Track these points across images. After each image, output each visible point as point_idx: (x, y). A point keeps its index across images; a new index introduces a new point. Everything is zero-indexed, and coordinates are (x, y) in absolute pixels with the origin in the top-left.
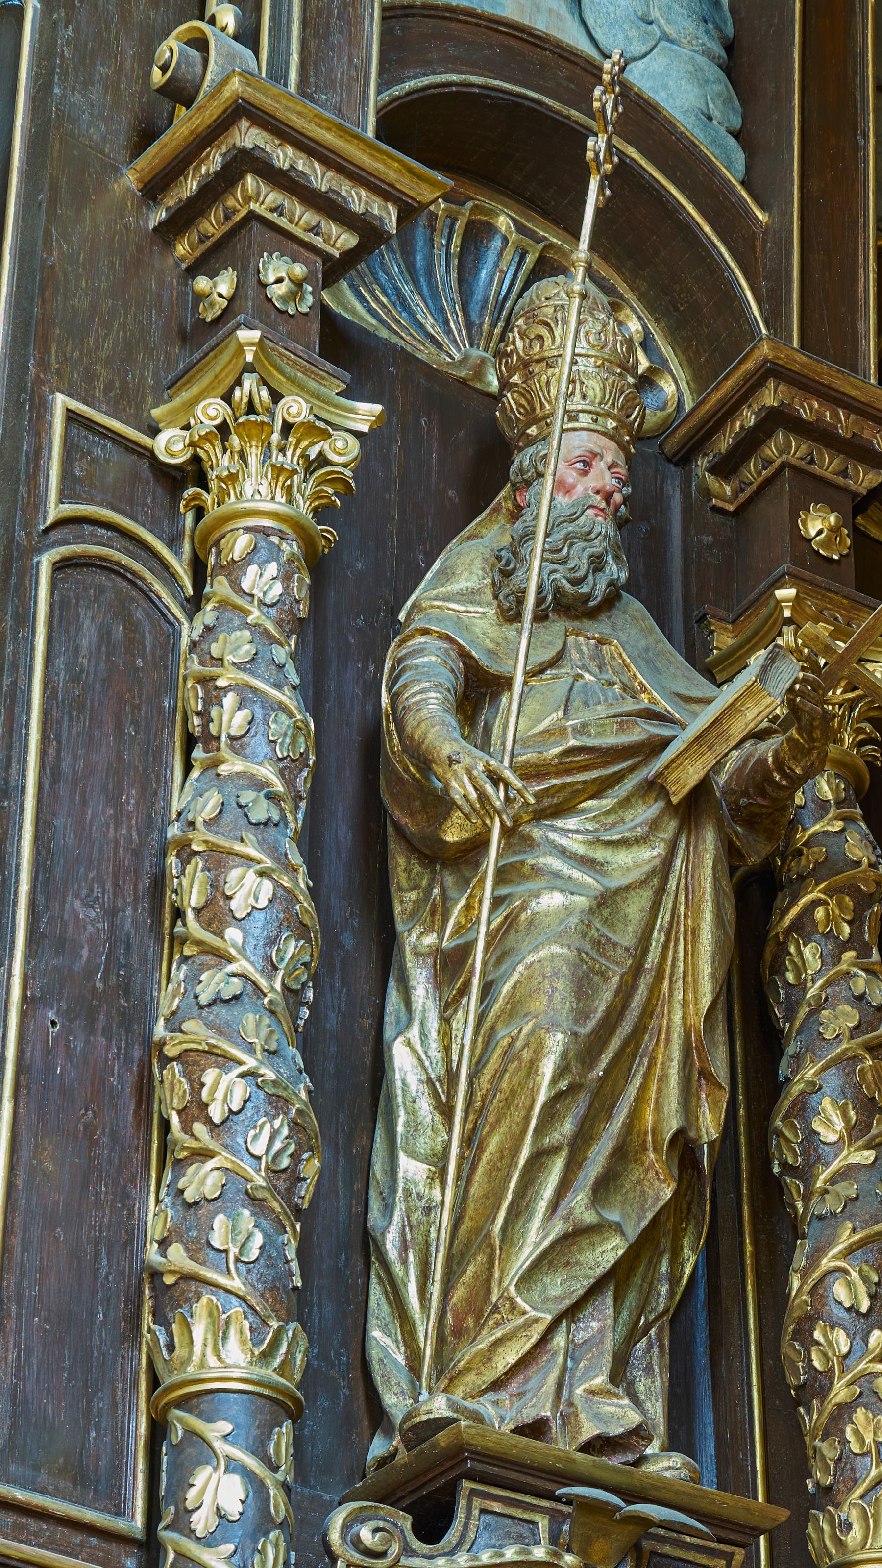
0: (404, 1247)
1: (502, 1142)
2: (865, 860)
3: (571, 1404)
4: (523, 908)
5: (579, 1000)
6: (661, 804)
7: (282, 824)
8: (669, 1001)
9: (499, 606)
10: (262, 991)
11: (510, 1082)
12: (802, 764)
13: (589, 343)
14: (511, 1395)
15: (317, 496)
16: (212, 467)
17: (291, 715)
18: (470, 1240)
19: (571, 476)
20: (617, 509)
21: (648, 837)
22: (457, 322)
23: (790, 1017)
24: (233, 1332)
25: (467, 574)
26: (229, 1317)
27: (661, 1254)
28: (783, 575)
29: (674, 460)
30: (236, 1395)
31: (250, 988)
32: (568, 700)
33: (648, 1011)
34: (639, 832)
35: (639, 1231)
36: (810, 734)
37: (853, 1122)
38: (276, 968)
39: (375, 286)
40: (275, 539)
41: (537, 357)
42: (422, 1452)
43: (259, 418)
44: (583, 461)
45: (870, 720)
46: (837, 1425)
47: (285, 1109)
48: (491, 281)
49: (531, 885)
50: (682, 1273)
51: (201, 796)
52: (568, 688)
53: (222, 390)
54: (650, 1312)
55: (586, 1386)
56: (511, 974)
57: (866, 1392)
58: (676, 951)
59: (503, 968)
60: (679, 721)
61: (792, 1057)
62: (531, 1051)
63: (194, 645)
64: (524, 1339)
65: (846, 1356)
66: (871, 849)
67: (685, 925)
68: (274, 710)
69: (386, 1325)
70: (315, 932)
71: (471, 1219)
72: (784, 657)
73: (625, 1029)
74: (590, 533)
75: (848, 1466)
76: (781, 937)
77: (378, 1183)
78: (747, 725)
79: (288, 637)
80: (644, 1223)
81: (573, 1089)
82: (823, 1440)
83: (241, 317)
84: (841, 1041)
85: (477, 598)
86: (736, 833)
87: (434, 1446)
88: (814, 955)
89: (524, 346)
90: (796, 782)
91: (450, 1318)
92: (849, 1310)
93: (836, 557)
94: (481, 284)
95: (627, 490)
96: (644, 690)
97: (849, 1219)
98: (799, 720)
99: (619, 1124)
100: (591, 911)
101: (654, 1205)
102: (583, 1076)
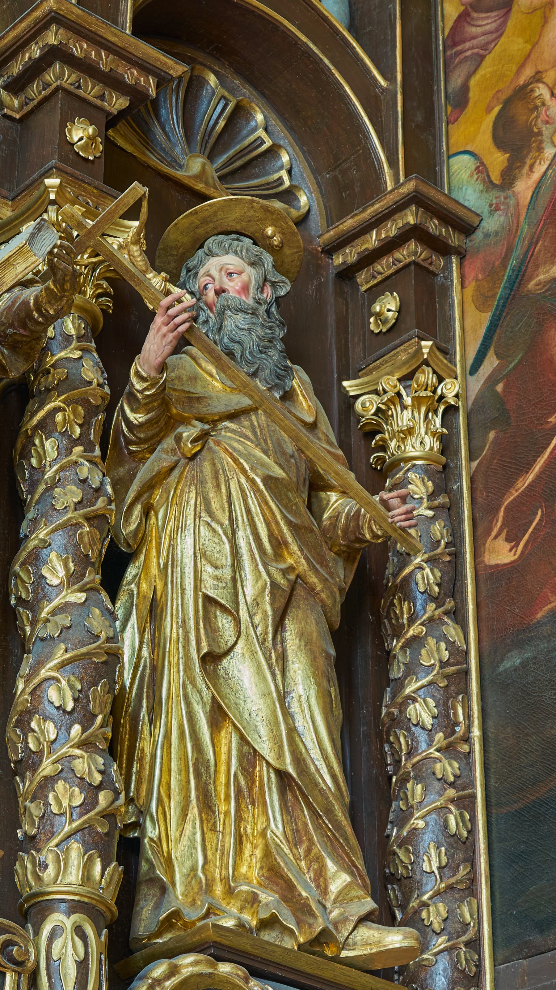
28: (51, 168)
36: (62, 286)
37: (72, 571)
45: (107, 279)
46: (43, 792)
57: (66, 769)
61: (31, 520)
65: (53, 742)
66: (100, 373)
75: (49, 822)
76: (29, 432)
78: (17, 275)
82: (31, 802)
84: (67, 511)
88: (53, 447)
90: (50, 320)
92: (58, 708)
93: (91, 158)
98: (55, 274)
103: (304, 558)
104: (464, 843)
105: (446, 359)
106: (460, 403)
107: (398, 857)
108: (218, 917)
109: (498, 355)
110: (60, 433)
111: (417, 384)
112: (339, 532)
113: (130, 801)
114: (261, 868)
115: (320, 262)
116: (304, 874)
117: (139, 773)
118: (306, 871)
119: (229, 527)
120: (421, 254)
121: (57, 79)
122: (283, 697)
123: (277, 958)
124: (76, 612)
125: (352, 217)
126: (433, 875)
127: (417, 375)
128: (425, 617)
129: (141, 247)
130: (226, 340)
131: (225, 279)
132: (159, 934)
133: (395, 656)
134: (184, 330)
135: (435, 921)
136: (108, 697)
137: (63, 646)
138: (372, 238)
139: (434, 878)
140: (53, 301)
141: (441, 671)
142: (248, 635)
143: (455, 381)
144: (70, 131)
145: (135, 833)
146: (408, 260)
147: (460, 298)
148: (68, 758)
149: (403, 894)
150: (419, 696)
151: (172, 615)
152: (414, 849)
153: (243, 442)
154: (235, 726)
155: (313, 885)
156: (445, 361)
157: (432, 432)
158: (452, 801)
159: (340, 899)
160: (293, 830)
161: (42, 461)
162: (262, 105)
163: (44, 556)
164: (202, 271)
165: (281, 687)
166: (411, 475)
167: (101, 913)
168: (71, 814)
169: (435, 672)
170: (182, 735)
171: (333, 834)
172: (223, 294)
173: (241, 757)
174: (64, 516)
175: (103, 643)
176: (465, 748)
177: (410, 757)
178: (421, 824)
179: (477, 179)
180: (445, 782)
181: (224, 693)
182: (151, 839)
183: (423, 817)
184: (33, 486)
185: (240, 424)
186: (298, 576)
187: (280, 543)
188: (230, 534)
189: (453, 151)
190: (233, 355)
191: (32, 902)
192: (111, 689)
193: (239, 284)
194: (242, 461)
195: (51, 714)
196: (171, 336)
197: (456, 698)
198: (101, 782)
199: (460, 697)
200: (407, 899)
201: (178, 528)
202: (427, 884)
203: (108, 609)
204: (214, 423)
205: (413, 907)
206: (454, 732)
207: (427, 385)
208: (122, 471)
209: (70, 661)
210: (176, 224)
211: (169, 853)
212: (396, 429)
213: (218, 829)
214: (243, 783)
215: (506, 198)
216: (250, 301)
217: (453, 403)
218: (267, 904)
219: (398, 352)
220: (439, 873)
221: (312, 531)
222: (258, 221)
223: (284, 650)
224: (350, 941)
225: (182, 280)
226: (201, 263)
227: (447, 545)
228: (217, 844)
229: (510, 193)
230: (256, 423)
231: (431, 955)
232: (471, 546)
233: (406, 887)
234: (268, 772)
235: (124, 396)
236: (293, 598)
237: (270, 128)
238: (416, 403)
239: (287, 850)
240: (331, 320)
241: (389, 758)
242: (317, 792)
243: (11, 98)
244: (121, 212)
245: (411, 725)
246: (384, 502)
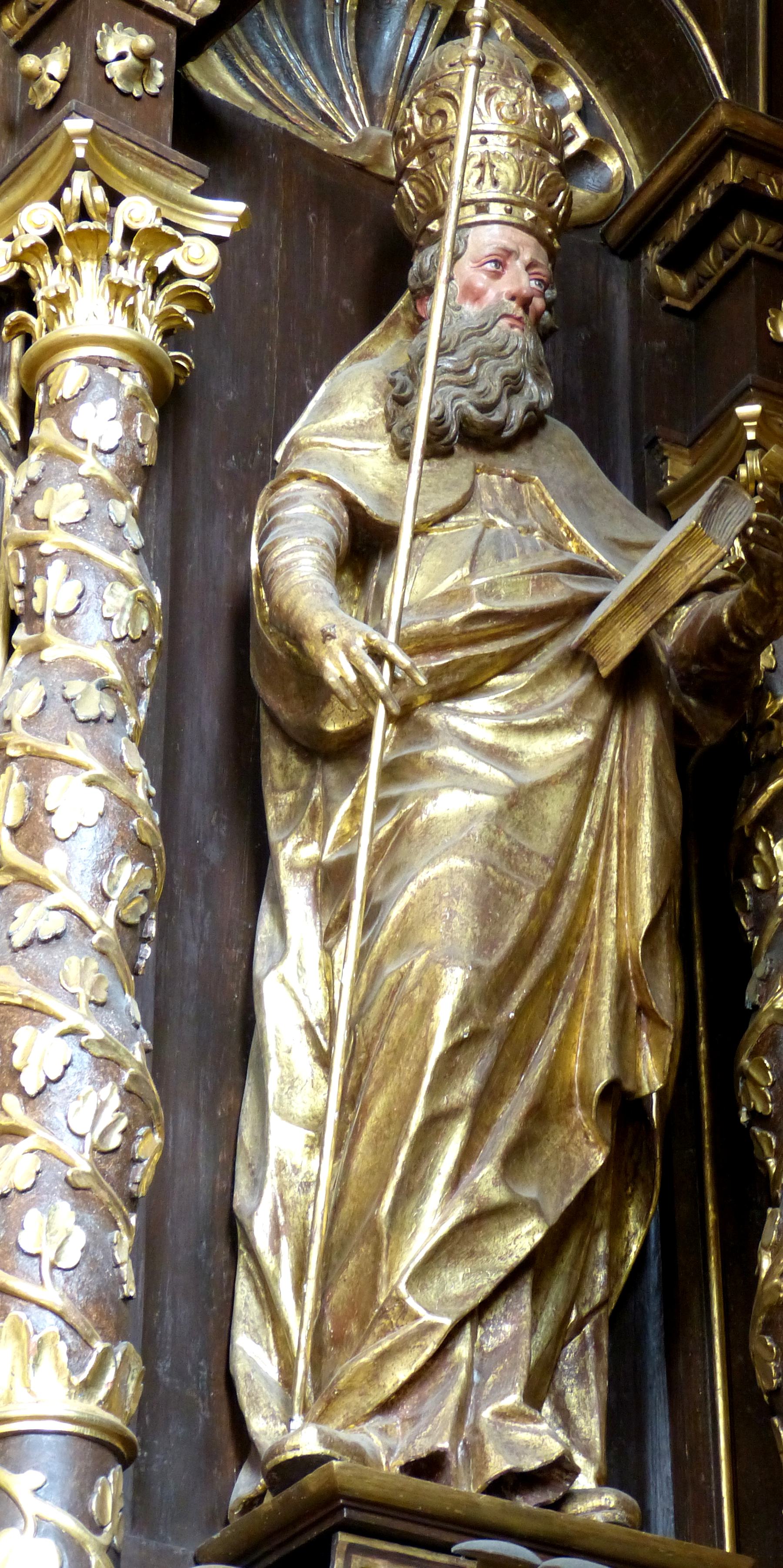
0: (276, 1233)
1: (389, 1103)
3: (476, 1430)
4: (417, 812)
5: (483, 925)
6: (588, 678)
7: (118, 720)
8: (600, 920)
9: (393, 441)
10: (90, 928)
11: (399, 1029)
13: (501, 117)
14: (404, 1420)
15: (167, 316)
16: (40, 286)
17: (130, 585)
18: (352, 1226)
19: (481, 280)
20: (538, 317)
21: (571, 718)
22: (354, 96)
23: (759, 929)
24: (47, 1355)
25: (355, 402)
26: (41, 1339)
27: (597, 1232)
28: (747, 388)
29: (619, 251)
30: (49, 1438)
31: (75, 924)
32: (475, 553)
33: (572, 934)
34: (561, 714)
35: (562, 1209)
36: (771, 586)
38: (107, 899)
39: (254, 57)
40: (114, 371)
41: (438, 137)
42: (287, 1499)
43: (92, 225)
44: (495, 261)
47: (115, 1073)
48: (396, 44)
49: (427, 784)
50: (628, 1250)
51: (20, 688)
52: (475, 538)
53: (51, 192)
54: (584, 1305)
55: (494, 1407)
56: (401, 895)
58: (608, 858)
59: (394, 885)
60: (613, 573)
62: (424, 991)
63: (17, 502)
64: (417, 1350)
67: (619, 826)
68: (109, 580)
69: (255, 1331)
70: (159, 852)
71: (354, 1200)
72: (736, 493)
73: (543, 958)
74: (503, 348)
76: (747, 831)
77: (247, 1153)
78: (688, 579)
79: (130, 489)
80: (570, 1198)
81: (476, 1036)
83: (72, 104)
85: (367, 431)
86: (688, 706)
87: (303, 1490)
89: (424, 124)
91: (329, 1326)
94: (384, 48)
95: (551, 294)
96: (571, 536)
98: (757, 569)
99: (537, 1076)
100: (500, 813)
101: (581, 1174)
102: (489, 1019)
121: (745, 239)
161: (771, 878)
184: (760, 921)
243: (675, 279)
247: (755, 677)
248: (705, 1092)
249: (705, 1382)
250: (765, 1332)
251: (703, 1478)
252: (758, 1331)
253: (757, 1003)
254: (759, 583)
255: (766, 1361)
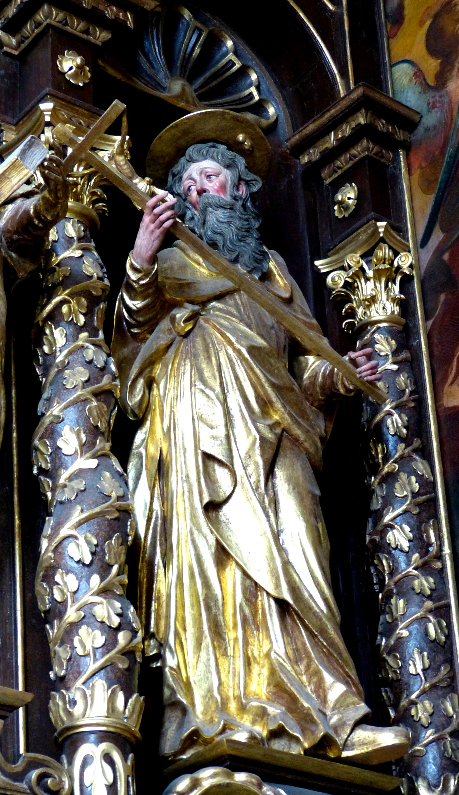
2: (95, 275)
12: (52, 213)
23: (45, 375)
36: (56, 194)
37: (84, 441)
45: (101, 187)
46: (69, 636)
57: (88, 615)
61: (46, 400)
65: (75, 592)
66: (99, 268)
75: (76, 663)
76: (40, 324)
78: (12, 187)
82: (60, 646)
84: (77, 390)
86: (11, 257)
88: (61, 335)
90: (48, 225)
92: (78, 562)
93: (81, 84)
97: (79, 503)
103: (288, 414)
104: (443, 647)
105: (400, 236)
106: (414, 272)
107: (388, 663)
108: (234, 731)
109: (443, 229)
110: (67, 322)
111: (376, 259)
112: (318, 389)
113: (149, 635)
114: (269, 685)
115: (289, 162)
116: (306, 687)
117: (157, 611)
118: (307, 684)
119: (220, 392)
120: (372, 150)
121: (46, 18)
122: (276, 535)
123: (286, 763)
124: (89, 476)
125: (312, 123)
126: (418, 676)
127: (376, 251)
128: (396, 456)
129: (126, 157)
130: (209, 233)
131: (205, 181)
132: (183, 751)
133: (373, 491)
134: (169, 226)
135: (423, 716)
136: (122, 550)
137: (79, 508)
138: (331, 139)
139: (419, 679)
140: (49, 208)
141: (413, 501)
142: (243, 484)
143: (408, 254)
144: (61, 63)
145: (157, 663)
146: (362, 155)
147: (408, 183)
148: (89, 605)
149: (395, 695)
150: (396, 524)
151: (177, 471)
152: (401, 655)
153: (229, 319)
154: (237, 563)
155: (314, 696)
156: (399, 238)
157: (392, 299)
158: (430, 611)
159: (338, 706)
160: (294, 649)
161: (53, 348)
162: (231, 33)
163: (59, 430)
164: (185, 176)
165: (275, 527)
166: (377, 336)
167: (126, 739)
168: (95, 655)
169: (408, 502)
170: (192, 575)
171: (328, 650)
172: (204, 194)
173: (245, 590)
174: (74, 394)
175: (114, 502)
176: (438, 565)
177: (392, 576)
178: (405, 633)
179: (415, 84)
180: (424, 595)
181: (226, 535)
182: (171, 668)
183: (406, 627)
184: (46, 369)
185: (226, 303)
186: (284, 430)
187: (266, 402)
188: (221, 397)
189: (394, 61)
190: (216, 244)
191: (65, 735)
192: (124, 542)
193: (218, 184)
194: (228, 335)
195: (72, 567)
196: (158, 232)
197: (427, 522)
198: (120, 624)
199: (431, 522)
200: (398, 699)
201: (177, 396)
202: (414, 685)
203: (118, 472)
204: (204, 303)
205: (404, 705)
206: (428, 552)
207: (385, 259)
208: (126, 351)
209: (87, 520)
210: (160, 137)
211: (188, 678)
212: (362, 297)
213: (229, 654)
214: (247, 612)
215: (440, 97)
216: (227, 198)
217: (408, 273)
218: (275, 717)
219: (359, 234)
220: (424, 675)
221: (292, 390)
222: (230, 129)
223: (275, 495)
224: (349, 742)
225: (169, 184)
226: (184, 169)
227: (411, 393)
228: (229, 667)
229: (443, 92)
230: (239, 302)
231: (421, 746)
232: (431, 392)
233: (396, 688)
234: (269, 601)
235: (123, 287)
236: (281, 449)
237: (239, 52)
238: (377, 275)
239: (289, 667)
240: (302, 210)
241: (375, 579)
242: (311, 615)
243: (9, 37)
244: (106, 127)
245: (391, 549)
246: (353, 361)
247: (47, 243)
248: (15, 458)
249: (11, 607)
250: (43, 581)
251: (9, 656)
252: (39, 580)
253: (44, 412)
254: (50, 192)
255: (43, 595)
